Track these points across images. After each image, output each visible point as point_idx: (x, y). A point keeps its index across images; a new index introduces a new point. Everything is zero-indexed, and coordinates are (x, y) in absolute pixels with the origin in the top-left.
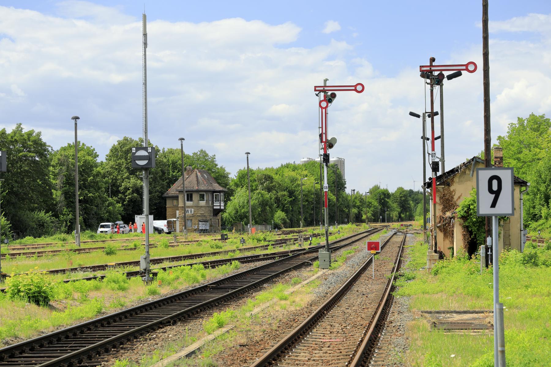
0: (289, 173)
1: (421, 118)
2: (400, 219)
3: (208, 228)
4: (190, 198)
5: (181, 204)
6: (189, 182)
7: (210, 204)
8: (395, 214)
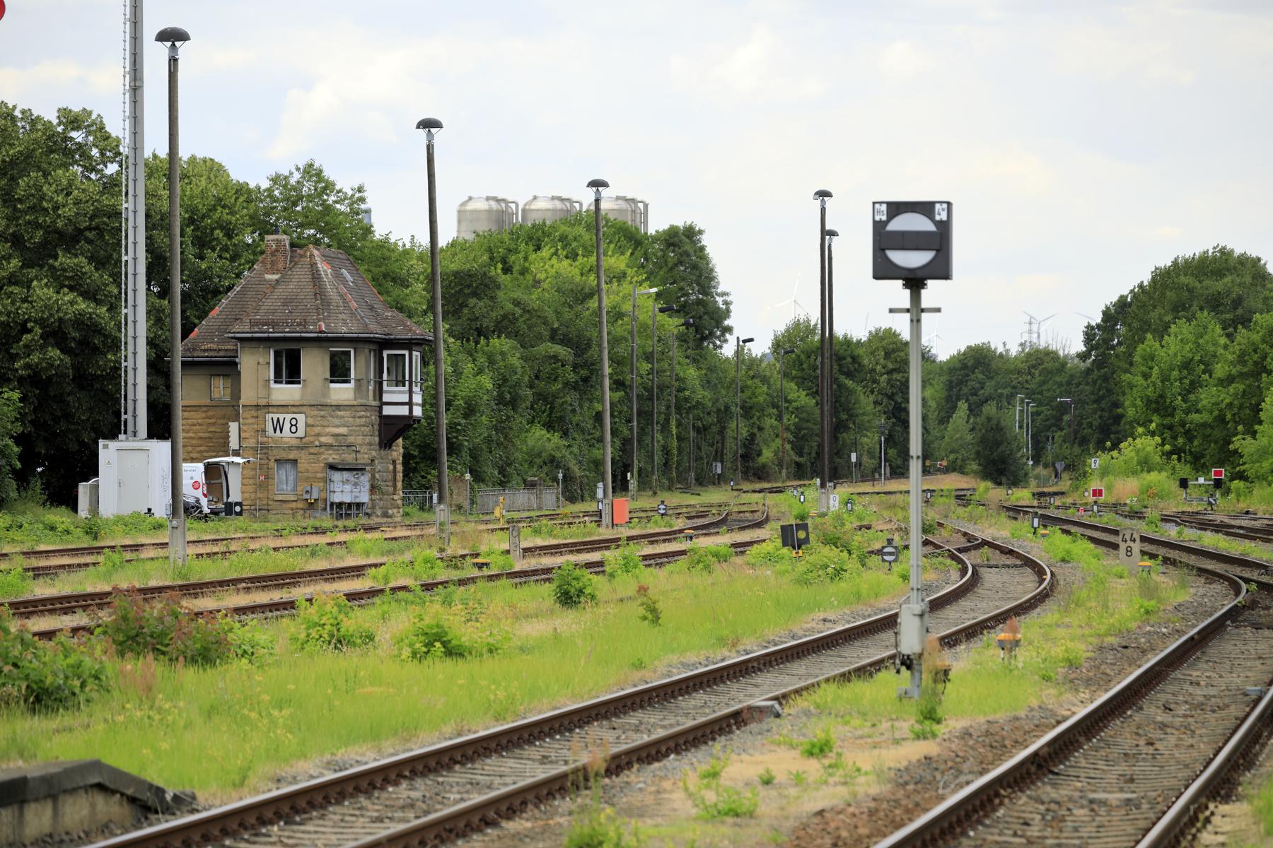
3: (364, 498)
4: (290, 370)
6: (286, 303)
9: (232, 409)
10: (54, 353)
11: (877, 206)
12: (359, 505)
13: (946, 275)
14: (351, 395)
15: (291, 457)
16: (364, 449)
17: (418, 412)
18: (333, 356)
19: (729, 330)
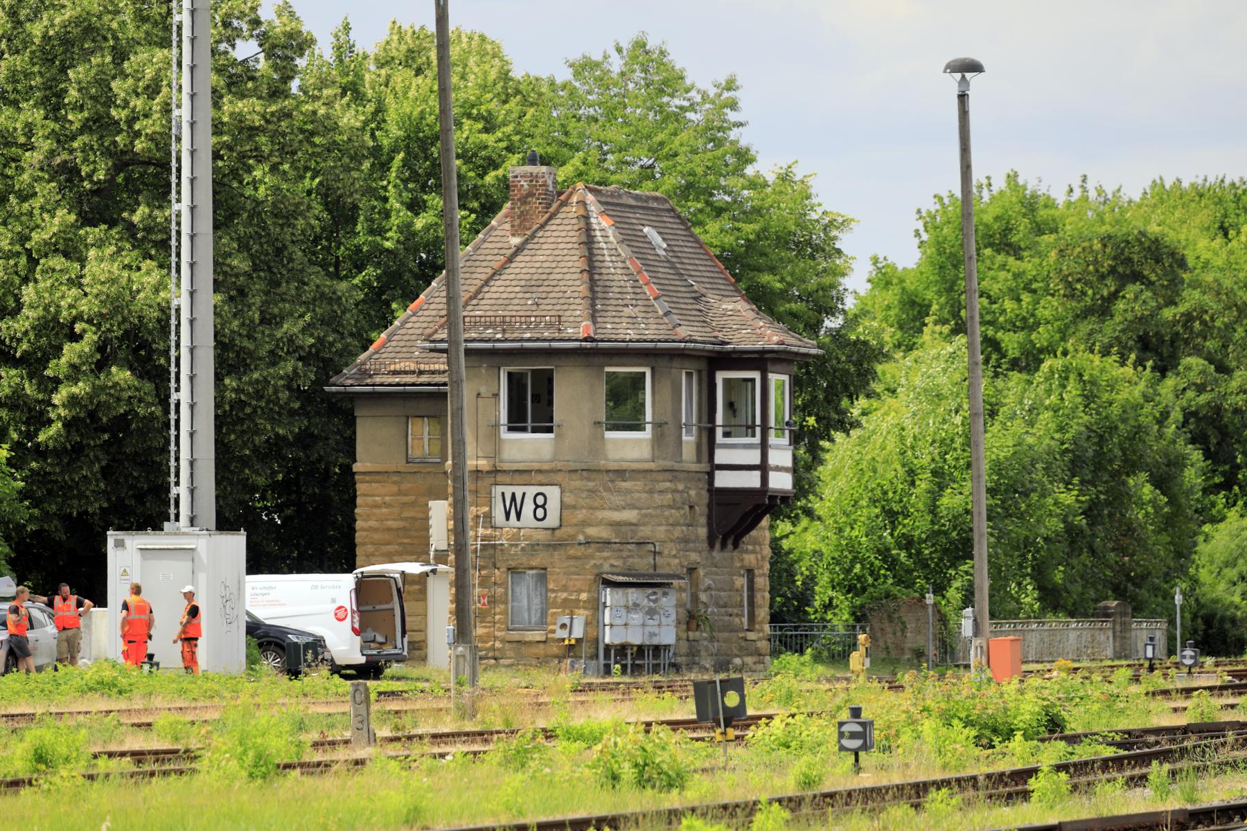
3: (668, 636)
4: (531, 405)
12: (657, 649)
14: (645, 452)
16: (670, 549)
18: (516, 382)
19: (224, 524)
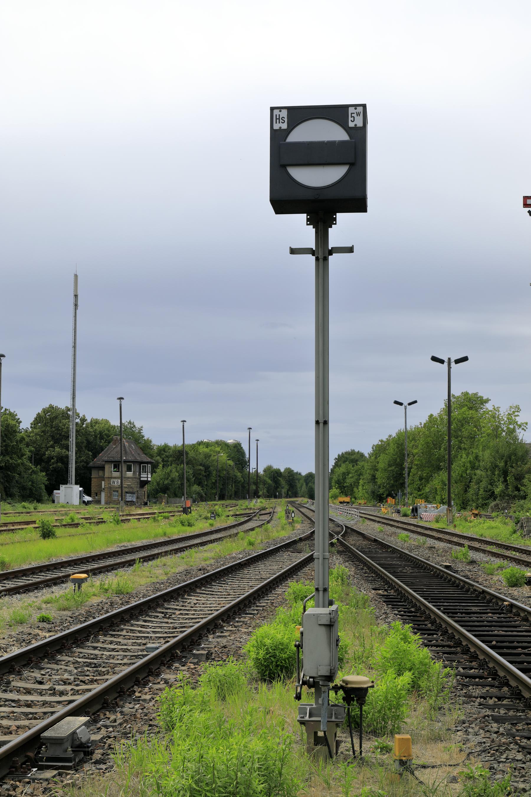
0: (203, 449)
1: (446, 364)
2: (287, 496)
3: (135, 500)
5: (107, 475)
7: (137, 475)
8: (284, 491)
9: (103, 478)
10: (60, 464)
11: (276, 112)
13: (359, 205)
14: (132, 475)
15: (117, 490)
17: (149, 479)
18: (128, 465)
